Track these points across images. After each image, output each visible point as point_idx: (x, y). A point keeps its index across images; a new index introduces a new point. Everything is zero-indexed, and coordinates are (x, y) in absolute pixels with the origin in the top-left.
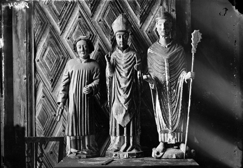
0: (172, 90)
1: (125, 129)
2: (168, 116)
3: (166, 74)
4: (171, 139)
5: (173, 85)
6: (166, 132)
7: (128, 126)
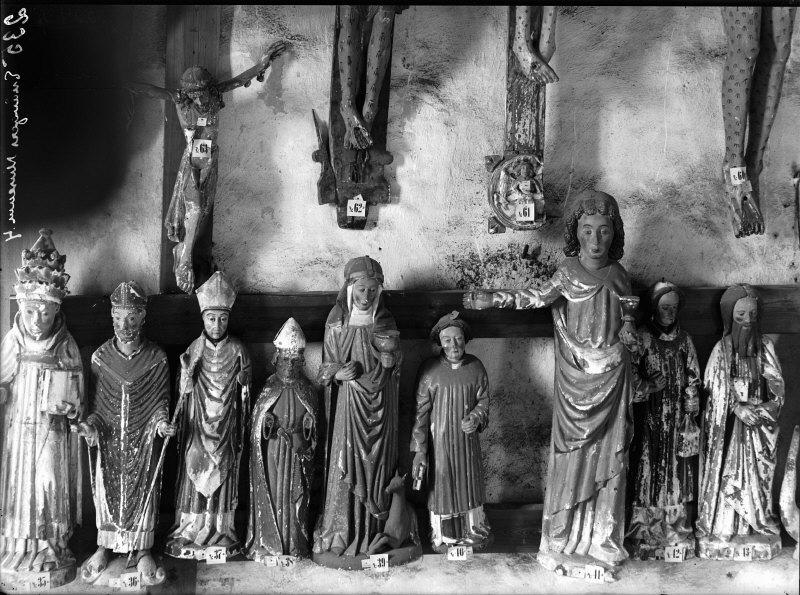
0: (132, 449)
1: (209, 500)
2: (119, 499)
3: (123, 416)
4: (120, 544)
5: (134, 439)
6: (111, 529)
7: (217, 493)
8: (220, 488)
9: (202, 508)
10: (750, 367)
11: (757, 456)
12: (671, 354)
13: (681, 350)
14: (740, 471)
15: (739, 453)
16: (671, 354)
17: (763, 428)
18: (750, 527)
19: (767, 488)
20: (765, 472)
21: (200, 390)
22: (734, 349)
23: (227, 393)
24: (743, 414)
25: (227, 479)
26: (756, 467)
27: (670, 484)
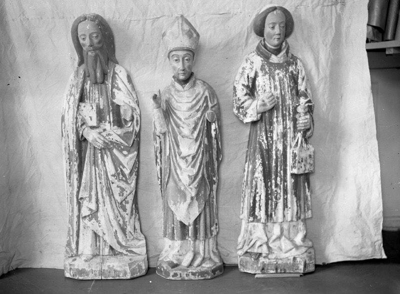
7: (196, 222)
8: (200, 215)
9: (184, 236)
10: (101, 93)
11: (111, 178)
12: (281, 75)
13: (292, 72)
14: (93, 193)
15: (91, 177)
16: (281, 75)
17: (115, 151)
18: (111, 248)
19: (125, 210)
20: (121, 194)
21: (173, 129)
22: (85, 77)
23: (198, 130)
24: (91, 136)
25: (205, 208)
26: (109, 189)
27: (285, 200)
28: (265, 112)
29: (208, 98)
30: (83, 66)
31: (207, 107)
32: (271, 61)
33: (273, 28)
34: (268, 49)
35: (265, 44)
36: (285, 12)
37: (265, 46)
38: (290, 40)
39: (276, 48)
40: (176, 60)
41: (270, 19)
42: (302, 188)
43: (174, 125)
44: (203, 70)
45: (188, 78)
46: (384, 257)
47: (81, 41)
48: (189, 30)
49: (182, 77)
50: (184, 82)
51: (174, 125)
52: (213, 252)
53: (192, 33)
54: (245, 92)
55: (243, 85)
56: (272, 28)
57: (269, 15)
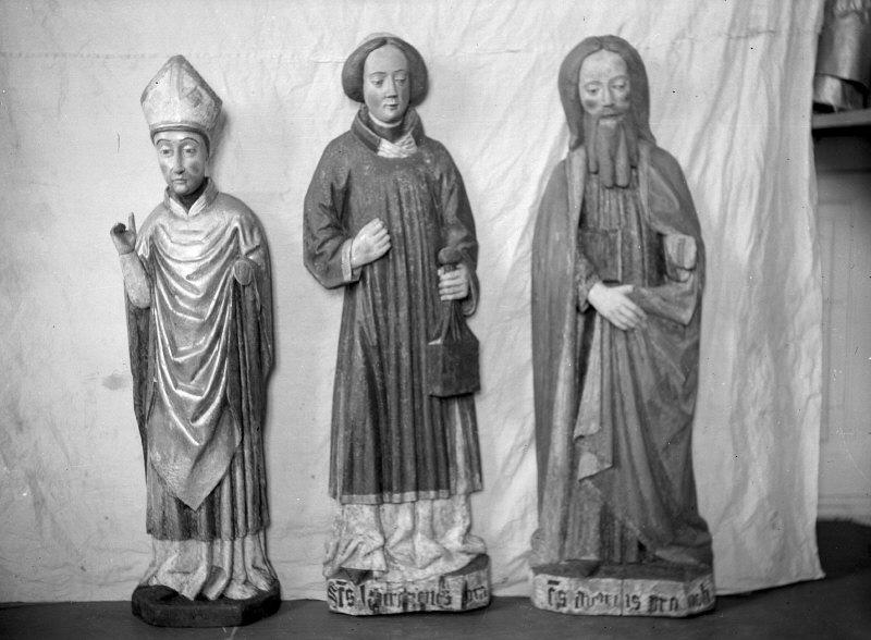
7: (212, 501)
25: (231, 471)
28: (371, 264)
29: (241, 232)
30: (581, 151)
31: (235, 254)
32: (380, 154)
33: (380, 83)
34: (376, 129)
35: (369, 118)
36: (406, 48)
37: (370, 124)
38: (421, 110)
39: (390, 126)
40: (166, 152)
41: (374, 63)
42: (395, 437)
43: (162, 290)
44: (227, 177)
45: (196, 190)
46: (820, 574)
47: (585, 96)
48: (195, 89)
49: (180, 188)
50: (187, 199)
51: (162, 290)
52: (254, 567)
53: (203, 90)
54: (326, 221)
55: (321, 205)
56: (378, 83)
57: (372, 54)
